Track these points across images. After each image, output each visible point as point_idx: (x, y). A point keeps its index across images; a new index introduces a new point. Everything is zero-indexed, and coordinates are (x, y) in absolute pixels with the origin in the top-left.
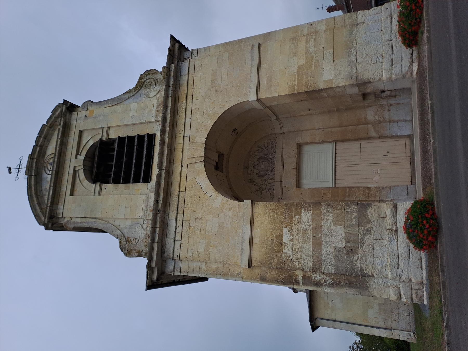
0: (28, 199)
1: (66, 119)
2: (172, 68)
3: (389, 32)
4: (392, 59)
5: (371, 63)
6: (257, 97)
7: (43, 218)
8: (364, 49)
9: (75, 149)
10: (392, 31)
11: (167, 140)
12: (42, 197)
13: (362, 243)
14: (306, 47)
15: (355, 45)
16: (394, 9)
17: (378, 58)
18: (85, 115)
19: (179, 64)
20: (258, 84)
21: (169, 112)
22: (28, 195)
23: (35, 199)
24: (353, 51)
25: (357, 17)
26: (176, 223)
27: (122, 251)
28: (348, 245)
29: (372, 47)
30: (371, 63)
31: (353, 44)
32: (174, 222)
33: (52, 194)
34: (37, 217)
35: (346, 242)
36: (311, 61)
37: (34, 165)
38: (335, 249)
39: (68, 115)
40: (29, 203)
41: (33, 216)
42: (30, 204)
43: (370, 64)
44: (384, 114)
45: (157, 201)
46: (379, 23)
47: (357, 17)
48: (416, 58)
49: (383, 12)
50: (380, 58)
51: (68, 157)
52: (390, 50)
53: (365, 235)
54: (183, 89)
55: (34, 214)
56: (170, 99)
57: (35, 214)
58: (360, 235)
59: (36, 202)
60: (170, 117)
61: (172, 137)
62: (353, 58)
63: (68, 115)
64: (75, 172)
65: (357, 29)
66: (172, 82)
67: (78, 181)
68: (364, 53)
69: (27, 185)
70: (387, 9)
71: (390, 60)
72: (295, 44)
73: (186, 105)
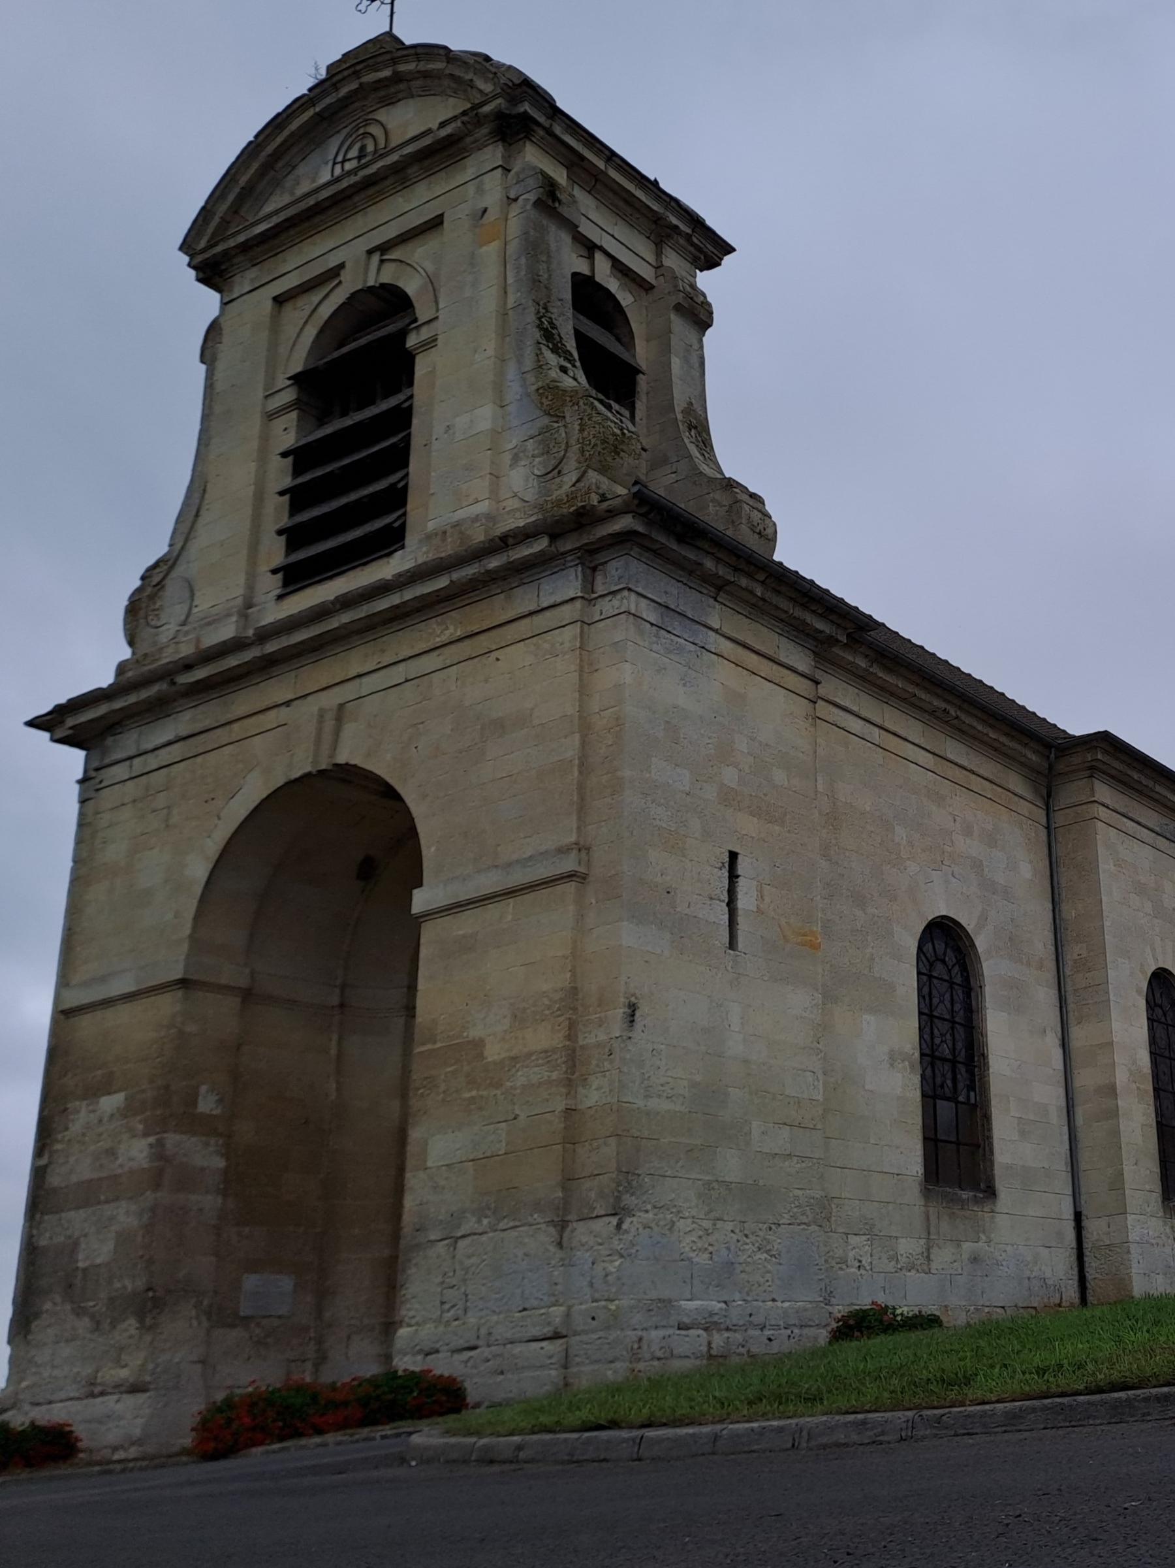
0: (244, 145)
1: (469, 133)
2: (535, 546)
3: (509, 1335)
4: (437, 1351)
5: (445, 1286)
6: (421, 917)
7: (203, 244)
8: (485, 1257)
9: (391, 232)
10: (511, 1343)
11: (333, 623)
12: (277, 184)
13: (79, 1312)
14: (530, 1054)
15: (502, 1225)
16: (587, 1344)
17: (454, 1306)
18: (485, 210)
19: (569, 558)
20: (456, 907)
21: (409, 594)
22: (256, 137)
23: (255, 166)
24: (485, 1221)
25: (597, 1217)
26: (169, 743)
27: (143, 578)
28: (80, 1275)
29: (484, 1285)
30: (445, 1286)
31: (506, 1221)
32: (169, 736)
33: (262, 234)
34: (201, 218)
35: (85, 1270)
36: (488, 1082)
37: (344, 91)
38: (76, 1244)
39: (484, 131)
40: (233, 159)
41: (201, 203)
42: (234, 164)
43: (443, 1283)
44: (33, 1357)
45: (188, 666)
46: (545, 1298)
47: (597, 1217)
48: (583, 1422)
49: (595, 1304)
50: (452, 1312)
51: (359, 223)
52: (462, 1343)
53: (92, 1317)
54: (498, 608)
55: (207, 202)
56: (442, 582)
57: (209, 207)
58: (91, 1304)
59: (243, 180)
60: (397, 607)
61: (359, 632)
62: (470, 1225)
63: (484, 131)
64: (335, 272)
65: (543, 1226)
66: (494, 563)
67: (315, 297)
68: (473, 1260)
69: (252, 139)
70: (593, 1318)
71: (438, 1346)
72: (547, 1012)
73: (451, 643)
